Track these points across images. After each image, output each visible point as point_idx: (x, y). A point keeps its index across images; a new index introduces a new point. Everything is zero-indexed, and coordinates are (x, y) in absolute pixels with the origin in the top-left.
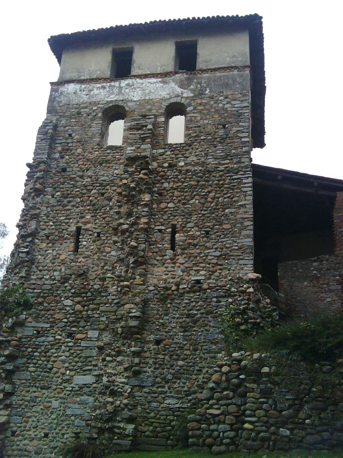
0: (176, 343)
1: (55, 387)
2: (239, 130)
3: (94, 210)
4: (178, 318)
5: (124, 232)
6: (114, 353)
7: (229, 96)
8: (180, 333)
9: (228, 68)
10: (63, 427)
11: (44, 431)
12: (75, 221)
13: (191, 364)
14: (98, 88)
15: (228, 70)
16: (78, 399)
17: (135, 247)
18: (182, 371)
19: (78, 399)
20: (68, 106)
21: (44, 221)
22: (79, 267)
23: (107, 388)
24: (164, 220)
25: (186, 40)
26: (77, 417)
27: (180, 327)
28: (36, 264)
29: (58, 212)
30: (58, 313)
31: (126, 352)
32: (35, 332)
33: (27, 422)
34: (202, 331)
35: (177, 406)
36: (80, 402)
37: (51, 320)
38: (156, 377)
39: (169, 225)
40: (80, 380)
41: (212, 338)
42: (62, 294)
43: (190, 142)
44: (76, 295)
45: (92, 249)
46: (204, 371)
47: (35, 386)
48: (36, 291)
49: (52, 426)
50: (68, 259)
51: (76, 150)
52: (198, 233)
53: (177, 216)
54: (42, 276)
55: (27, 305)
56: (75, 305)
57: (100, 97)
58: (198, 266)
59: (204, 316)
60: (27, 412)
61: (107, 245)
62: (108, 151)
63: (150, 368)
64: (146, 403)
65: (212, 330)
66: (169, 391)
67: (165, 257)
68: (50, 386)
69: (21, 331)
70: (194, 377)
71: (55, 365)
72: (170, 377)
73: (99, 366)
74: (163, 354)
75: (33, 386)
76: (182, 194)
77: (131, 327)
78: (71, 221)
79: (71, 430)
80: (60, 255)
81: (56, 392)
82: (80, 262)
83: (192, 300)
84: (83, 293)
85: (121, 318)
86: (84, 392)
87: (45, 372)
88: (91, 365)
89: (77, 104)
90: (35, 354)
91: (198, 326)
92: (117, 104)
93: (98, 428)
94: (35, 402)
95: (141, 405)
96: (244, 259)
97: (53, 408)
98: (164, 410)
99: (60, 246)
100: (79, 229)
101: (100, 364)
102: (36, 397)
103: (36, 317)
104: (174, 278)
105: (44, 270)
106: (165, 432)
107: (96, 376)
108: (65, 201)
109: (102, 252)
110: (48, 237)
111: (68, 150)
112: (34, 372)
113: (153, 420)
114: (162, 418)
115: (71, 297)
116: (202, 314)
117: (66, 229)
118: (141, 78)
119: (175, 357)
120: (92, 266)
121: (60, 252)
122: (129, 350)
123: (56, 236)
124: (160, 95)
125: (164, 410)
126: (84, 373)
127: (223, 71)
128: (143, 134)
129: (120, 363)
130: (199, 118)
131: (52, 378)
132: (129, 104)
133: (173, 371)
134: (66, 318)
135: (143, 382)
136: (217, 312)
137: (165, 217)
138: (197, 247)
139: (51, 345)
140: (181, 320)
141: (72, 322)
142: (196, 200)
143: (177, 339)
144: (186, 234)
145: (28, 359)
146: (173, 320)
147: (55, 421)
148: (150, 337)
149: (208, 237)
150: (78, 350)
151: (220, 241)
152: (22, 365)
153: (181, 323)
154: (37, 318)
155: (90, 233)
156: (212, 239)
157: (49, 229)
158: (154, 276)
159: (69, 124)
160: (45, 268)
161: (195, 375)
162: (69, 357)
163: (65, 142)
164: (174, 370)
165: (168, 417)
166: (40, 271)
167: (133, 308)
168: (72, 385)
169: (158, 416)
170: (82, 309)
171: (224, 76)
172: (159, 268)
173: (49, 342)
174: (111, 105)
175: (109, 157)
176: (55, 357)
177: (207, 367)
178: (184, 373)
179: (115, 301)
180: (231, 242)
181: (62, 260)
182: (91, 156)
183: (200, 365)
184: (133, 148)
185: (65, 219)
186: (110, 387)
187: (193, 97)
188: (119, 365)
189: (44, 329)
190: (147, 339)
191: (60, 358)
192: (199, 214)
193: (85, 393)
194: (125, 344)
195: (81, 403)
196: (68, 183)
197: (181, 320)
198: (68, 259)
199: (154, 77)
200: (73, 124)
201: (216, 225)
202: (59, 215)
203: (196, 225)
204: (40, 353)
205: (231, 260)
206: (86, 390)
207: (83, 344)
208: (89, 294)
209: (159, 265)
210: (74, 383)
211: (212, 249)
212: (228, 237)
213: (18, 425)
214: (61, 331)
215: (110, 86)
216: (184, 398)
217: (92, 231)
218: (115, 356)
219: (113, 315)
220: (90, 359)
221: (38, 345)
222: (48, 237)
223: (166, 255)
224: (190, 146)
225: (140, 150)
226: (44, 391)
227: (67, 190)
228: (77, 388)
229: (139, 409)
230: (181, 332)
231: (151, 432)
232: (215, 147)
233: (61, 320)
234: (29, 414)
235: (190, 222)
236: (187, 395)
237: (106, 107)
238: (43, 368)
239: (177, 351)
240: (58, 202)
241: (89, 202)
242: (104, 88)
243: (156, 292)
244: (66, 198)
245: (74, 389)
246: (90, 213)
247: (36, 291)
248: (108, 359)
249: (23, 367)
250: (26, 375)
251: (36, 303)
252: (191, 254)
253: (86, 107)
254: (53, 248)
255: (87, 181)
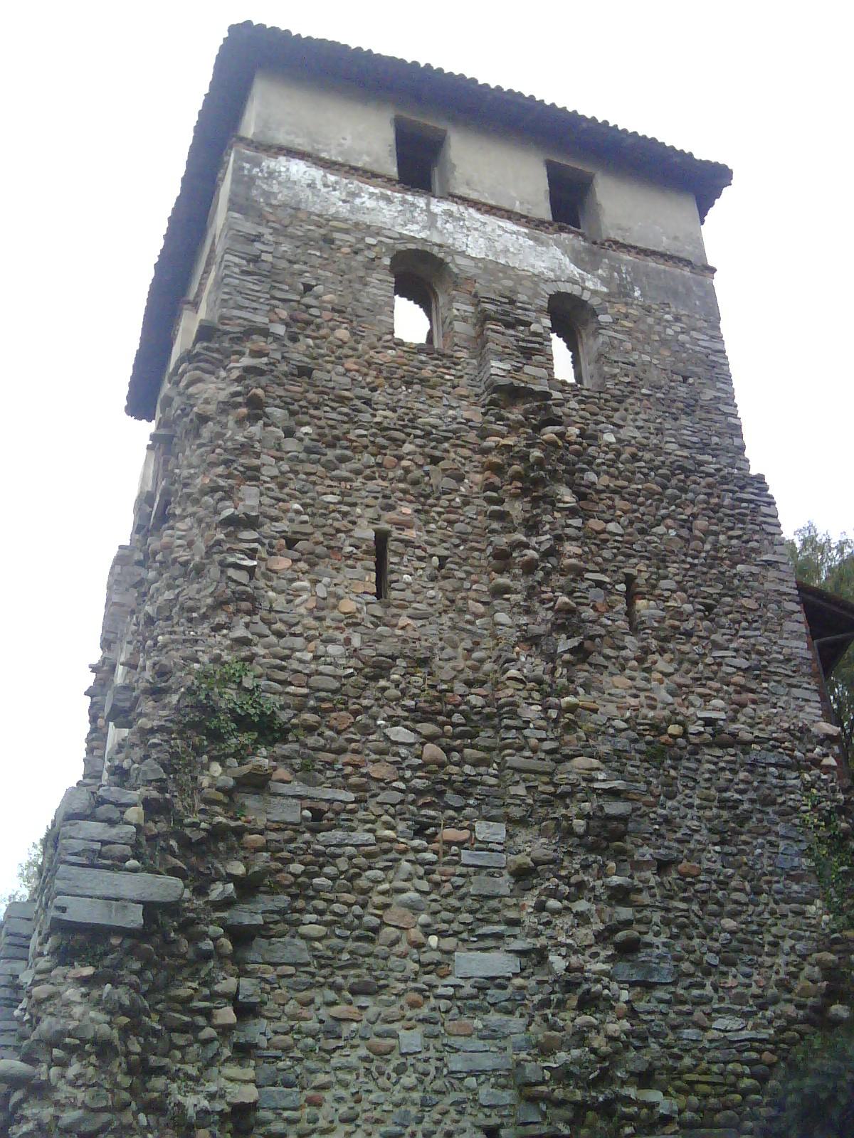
0: (709, 872)
1: (401, 986)
2: (719, 398)
3: (422, 495)
4: (700, 808)
5: (530, 567)
6: (565, 889)
7: (684, 319)
8: (710, 847)
9: (671, 257)
10: (445, 1113)
11: (383, 1129)
12: (370, 513)
13: (755, 927)
14: (372, 195)
15: (671, 263)
16: (478, 1023)
17: (571, 611)
18: (735, 943)
19: (478, 1023)
20: (293, 212)
21: (271, 494)
22: (405, 641)
23: (570, 986)
24: (605, 559)
25: (564, 162)
26: (483, 1078)
27: (710, 830)
28: (264, 613)
29: (313, 478)
30: (374, 762)
31: (593, 889)
32: (307, 813)
33: (317, 1103)
34: (762, 846)
35: (745, 1034)
36: (486, 1033)
37: (354, 780)
38: (679, 959)
39: (621, 577)
40: (475, 964)
41: (787, 865)
42: (374, 709)
43: (619, 393)
44: (418, 715)
45: (433, 598)
46: (786, 945)
47: (333, 986)
48: (291, 689)
49: (407, 1112)
50: (363, 615)
51: (333, 329)
52: (688, 607)
53: (634, 556)
54: (287, 652)
55: (268, 730)
56: (423, 744)
57: (381, 218)
58: (704, 686)
59: (758, 806)
60: (312, 1072)
61: (471, 594)
62: (423, 358)
63: (657, 934)
64: (668, 1031)
65: (782, 845)
66: (716, 996)
67: (623, 653)
68: (382, 982)
69: (257, 805)
70: (768, 961)
71: (389, 916)
72: (711, 958)
73: (527, 923)
74: (684, 900)
75: (322, 985)
76: (635, 507)
77: (610, 818)
78: (358, 510)
79: (471, 1118)
80: (339, 598)
81: (403, 1001)
82: (403, 628)
83: (722, 765)
84: (440, 713)
85: (570, 795)
86: (492, 1001)
87: (358, 939)
88: (498, 923)
89: (319, 216)
90: (316, 881)
91: (749, 831)
92: (428, 249)
93: (575, 1103)
94: (339, 1037)
95: (656, 1035)
96: (800, 687)
97: (403, 1055)
98: (717, 1048)
99: (334, 572)
100: (382, 539)
101: (530, 920)
102: (338, 1020)
103: (305, 768)
104: (653, 708)
105: (294, 635)
106: (728, 1108)
107: (521, 953)
108: (331, 454)
109: (462, 611)
110: (291, 543)
111: (308, 323)
112: (319, 939)
113: (693, 1077)
114: (715, 1068)
115: (406, 719)
116: (752, 801)
117: (347, 532)
118: (479, 210)
119: (712, 907)
120: (440, 644)
121: (340, 591)
122: (599, 882)
123: (317, 543)
124: (533, 266)
125: (717, 1048)
126: (481, 944)
127: (662, 261)
128: (524, 340)
129: (583, 919)
130: (629, 346)
131: (386, 959)
132: (460, 260)
133: (716, 945)
134: (402, 779)
135: (651, 972)
136: (784, 802)
137: (607, 554)
138: (694, 639)
139: (368, 856)
140: (708, 813)
141: (419, 793)
142: (668, 527)
143: (709, 860)
144: (662, 605)
145: (294, 897)
146: (691, 813)
147: (416, 1096)
148: (641, 850)
149: (712, 620)
150: (454, 875)
151: (741, 633)
152: (276, 917)
153: (709, 820)
154: (306, 771)
155: (419, 552)
156: (723, 627)
157: (292, 521)
158: (606, 696)
159: (303, 258)
160: (298, 629)
161: (768, 955)
162: (428, 893)
163: (298, 302)
164: (717, 940)
165: (730, 1066)
166: (280, 635)
167: (598, 769)
168: (450, 980)
169: (704, 1065)
170: (444, 757)
171: (665, 271)
172: (615, 678)
173: (357, 846)
174: (412, 246)
175: (426, 373)
176: (383, 893)
177: (791, 937)
178: (741, 951)
179: (548, 745)
180: (766, 641)
181: (349, 615)
182: (379, 358)
183: (774, 930)
184: (507, 367)
185: (340, 503)
186: (579, 984)
187: (608, 294)
188: (578, 925)
189: (336, 806)
190: (636, 857)
191: (404, 896)
192: (684, 562)
193: (493, 1005)
194: (589, 866)
195: (492, 1034)
196: (333, 409)
197: (708, 813)
198: (363, 615)
199: (509, 218)
200: (317, 262)
201: (725, 595)
202: (319, 488)
203: (681, 587)
204: (333, 879)
205: (773, 684)
206: (494, 994)
207: (466, 857)
208: (456, 718)
209: (612, 668)
210: (459, 972)
211: (727, 649)
212: (756, 629)
213: (286, 1114)
214: (393, 816)
215: (404, 202)
216: (755, 1013)
217: (425, 550)
218: (567, 898)
219: (547, 784)
220: (494, 903)
221: (323, 854)
222: (291, 543)
223: (624, 648)
224: (620, 402)
225: (518, 375)
226: (363, 1000)
227: (332, 427)
228: (468, 990)
229: (655, 1046)
230: (715, 844)
231: (697, 1111)
232: (676, 419)
233: (386, 785)
234: (321, 1078)
235: (666, 578)
236: (763, 1007)
237: (401, 247)
238: (348, 927)
239: (715, 891)
240: (308, 450)
241: (400, 472)
242: (389, 200)
243: (633, 735)
244: (331, 446)
245: (463, 992)
246: (411, 502)
247: (291, 689)
248: (553, 903)
249: (276, 922)
250: (295, 949)
251: (295, 726)
252: (683, 653)
253: (346, 231)
254: (312, 576)
255: (386, 417)
